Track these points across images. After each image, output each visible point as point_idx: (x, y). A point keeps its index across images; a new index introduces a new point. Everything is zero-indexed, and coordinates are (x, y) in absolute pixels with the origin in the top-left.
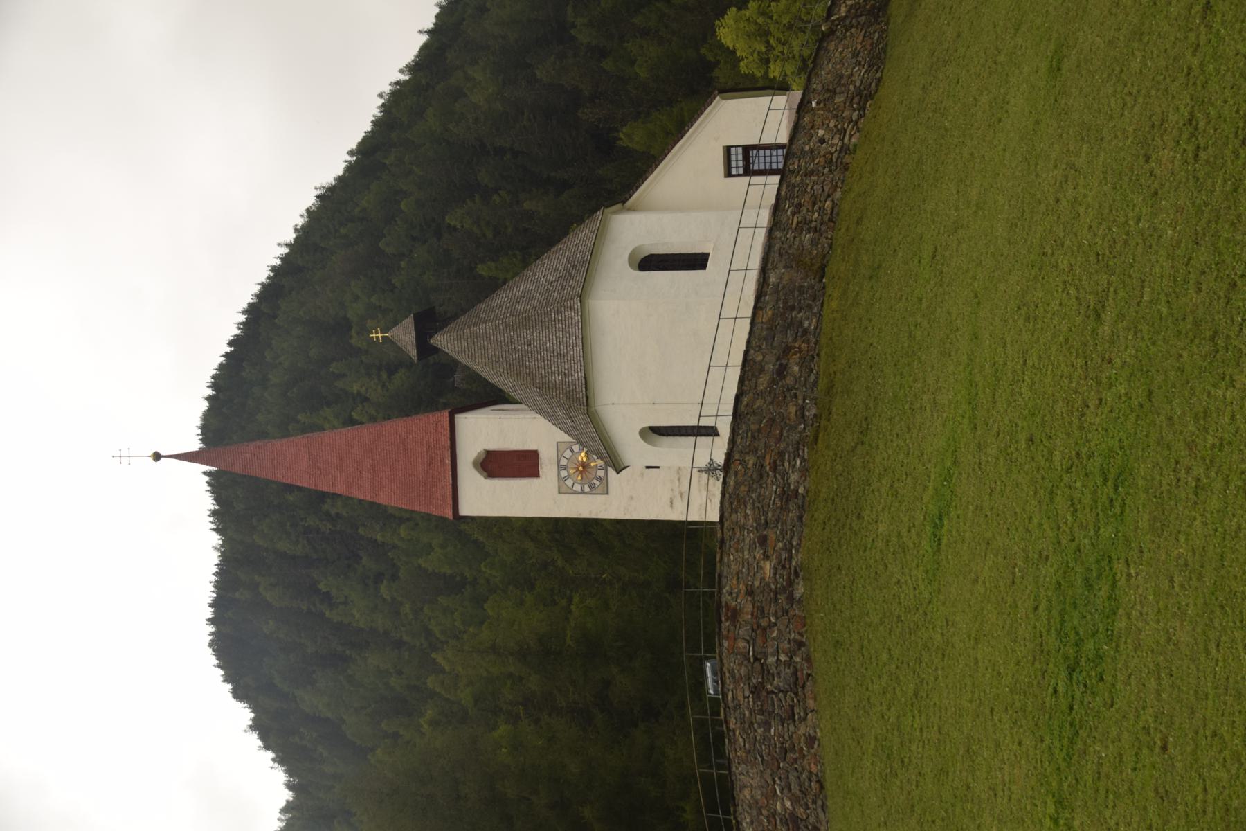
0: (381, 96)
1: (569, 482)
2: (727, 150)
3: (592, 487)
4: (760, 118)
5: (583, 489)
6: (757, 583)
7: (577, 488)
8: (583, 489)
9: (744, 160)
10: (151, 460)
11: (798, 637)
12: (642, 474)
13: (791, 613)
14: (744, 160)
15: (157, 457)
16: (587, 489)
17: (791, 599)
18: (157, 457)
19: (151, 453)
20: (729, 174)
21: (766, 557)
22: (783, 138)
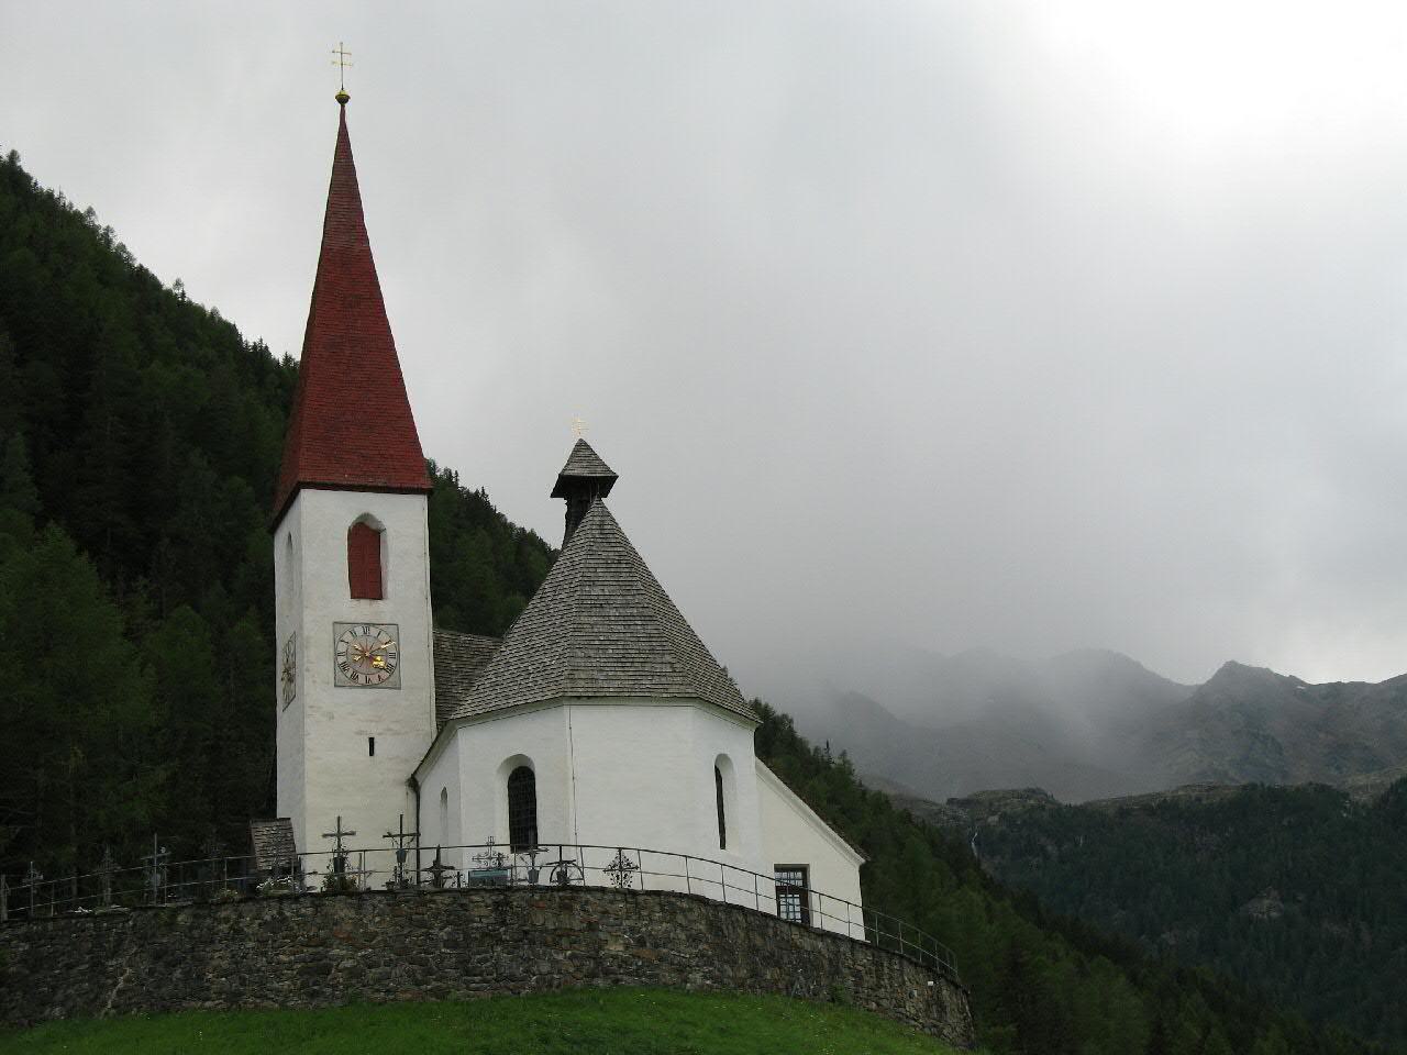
0: (178, 284)
1: (348, 637)
2: (804, 869)
3: (344, 667)
4: (839, 903)
5: (339, 654)
6: (602, 936)
7: (342, 648)
8: (339, 654)
9: (794, 882)
10: (337, 92)
11: (556, 982)
12: (360, 733)
13: (579, 975)
14: (794, 882)
15: (343, 100)
16: (341, 660)
17: (593, 975)
18: (343, 100)
19: (347, 92)
20: (778, 868)
21: (627, 947)
22: (816, 922)
